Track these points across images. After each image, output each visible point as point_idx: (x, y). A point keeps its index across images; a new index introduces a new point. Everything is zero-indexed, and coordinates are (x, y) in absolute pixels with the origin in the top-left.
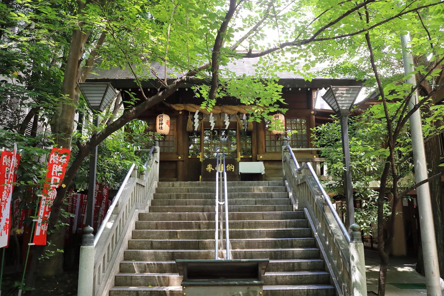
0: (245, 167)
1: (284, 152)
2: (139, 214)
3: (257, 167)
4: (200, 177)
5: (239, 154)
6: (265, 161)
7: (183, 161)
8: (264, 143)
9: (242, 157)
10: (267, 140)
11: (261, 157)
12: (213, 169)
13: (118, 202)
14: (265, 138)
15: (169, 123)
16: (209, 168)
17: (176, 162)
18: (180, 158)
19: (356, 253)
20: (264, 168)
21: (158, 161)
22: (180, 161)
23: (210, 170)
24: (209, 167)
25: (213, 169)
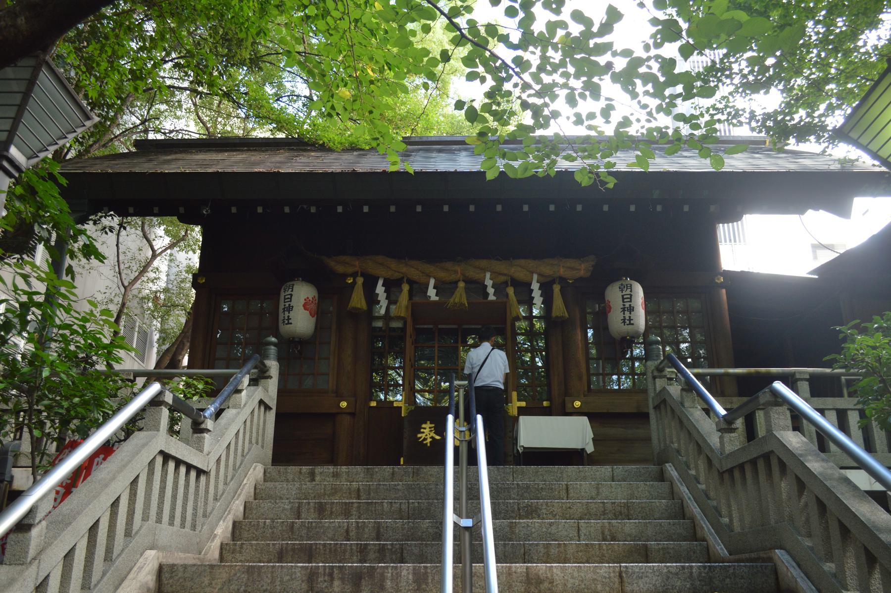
0: (535, 431)
1: (654, 378)
2: (161, 570)
3: (571, 431)
4: (402, 459)
5: (514, 395)
6: (593, 417)
7: (353, 414)
8: (583, 366)
9: (523, 404)
10: (592, 372)
11: (577, 404)
12: (438, 437)
13: (31, 512)
14: (588, 369)
15: (313, 307)
16: (427, 433)
17: (333, 416)
18: (344, 404)
19: (22, 208)
20: (590, 434)
21: (273, 404)
22: (342, 412)
23: (429, 440)
24: (427, 431)
25: (438, 437)
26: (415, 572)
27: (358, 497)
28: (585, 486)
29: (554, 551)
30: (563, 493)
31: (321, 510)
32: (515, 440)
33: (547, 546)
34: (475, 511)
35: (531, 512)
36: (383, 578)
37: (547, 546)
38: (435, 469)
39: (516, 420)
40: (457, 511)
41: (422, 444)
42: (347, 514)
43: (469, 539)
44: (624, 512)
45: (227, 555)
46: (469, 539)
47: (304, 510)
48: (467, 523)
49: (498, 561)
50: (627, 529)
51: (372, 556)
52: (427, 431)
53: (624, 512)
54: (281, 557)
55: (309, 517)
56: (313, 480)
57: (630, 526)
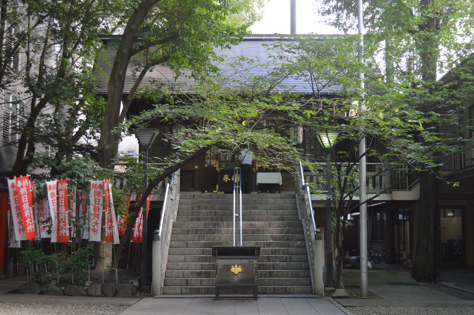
7: (199, 171)
16: (226, 178)
18: (196, 167)
22: (196, 170)
26: (227, 223)
27: (208, 204)
28: (272, 201)
29: (260, 218)
30: (266, 202)
31: (199, 207)
32: (256, 180)
33: (258, 217)
34: (239, 213)
35: (256, 208)
36: (220, 225)
37: (258, 217)
38: (230, 195)
39: (256, 174)
40: (236, 213)
41: (224, 182)
42: (206, 209)
43: (238, 219)
44: (281, 208)
45: (179, 220)
46: (238, 219)
47: (194, 207)
48: (237, 215)
49: (242, 221)
50: (280, 212)
51: (215, 219)
52: (226, 177)
53: (281, 208)
54: (192, 220)
55: (196, 210)
56: (194, 198)
57: (281, 212)
